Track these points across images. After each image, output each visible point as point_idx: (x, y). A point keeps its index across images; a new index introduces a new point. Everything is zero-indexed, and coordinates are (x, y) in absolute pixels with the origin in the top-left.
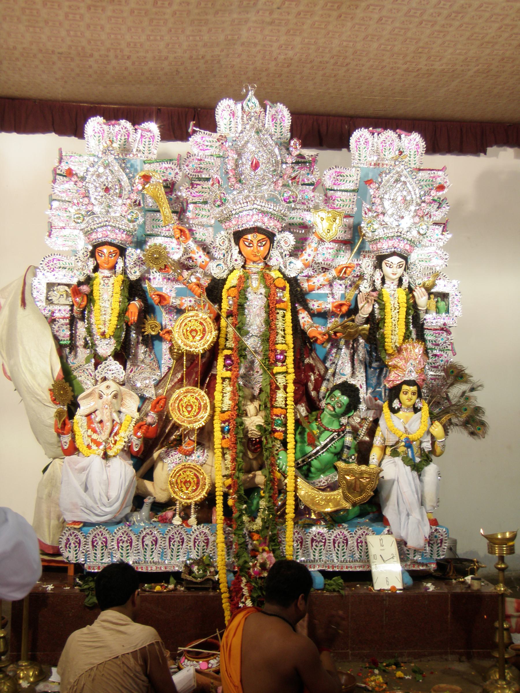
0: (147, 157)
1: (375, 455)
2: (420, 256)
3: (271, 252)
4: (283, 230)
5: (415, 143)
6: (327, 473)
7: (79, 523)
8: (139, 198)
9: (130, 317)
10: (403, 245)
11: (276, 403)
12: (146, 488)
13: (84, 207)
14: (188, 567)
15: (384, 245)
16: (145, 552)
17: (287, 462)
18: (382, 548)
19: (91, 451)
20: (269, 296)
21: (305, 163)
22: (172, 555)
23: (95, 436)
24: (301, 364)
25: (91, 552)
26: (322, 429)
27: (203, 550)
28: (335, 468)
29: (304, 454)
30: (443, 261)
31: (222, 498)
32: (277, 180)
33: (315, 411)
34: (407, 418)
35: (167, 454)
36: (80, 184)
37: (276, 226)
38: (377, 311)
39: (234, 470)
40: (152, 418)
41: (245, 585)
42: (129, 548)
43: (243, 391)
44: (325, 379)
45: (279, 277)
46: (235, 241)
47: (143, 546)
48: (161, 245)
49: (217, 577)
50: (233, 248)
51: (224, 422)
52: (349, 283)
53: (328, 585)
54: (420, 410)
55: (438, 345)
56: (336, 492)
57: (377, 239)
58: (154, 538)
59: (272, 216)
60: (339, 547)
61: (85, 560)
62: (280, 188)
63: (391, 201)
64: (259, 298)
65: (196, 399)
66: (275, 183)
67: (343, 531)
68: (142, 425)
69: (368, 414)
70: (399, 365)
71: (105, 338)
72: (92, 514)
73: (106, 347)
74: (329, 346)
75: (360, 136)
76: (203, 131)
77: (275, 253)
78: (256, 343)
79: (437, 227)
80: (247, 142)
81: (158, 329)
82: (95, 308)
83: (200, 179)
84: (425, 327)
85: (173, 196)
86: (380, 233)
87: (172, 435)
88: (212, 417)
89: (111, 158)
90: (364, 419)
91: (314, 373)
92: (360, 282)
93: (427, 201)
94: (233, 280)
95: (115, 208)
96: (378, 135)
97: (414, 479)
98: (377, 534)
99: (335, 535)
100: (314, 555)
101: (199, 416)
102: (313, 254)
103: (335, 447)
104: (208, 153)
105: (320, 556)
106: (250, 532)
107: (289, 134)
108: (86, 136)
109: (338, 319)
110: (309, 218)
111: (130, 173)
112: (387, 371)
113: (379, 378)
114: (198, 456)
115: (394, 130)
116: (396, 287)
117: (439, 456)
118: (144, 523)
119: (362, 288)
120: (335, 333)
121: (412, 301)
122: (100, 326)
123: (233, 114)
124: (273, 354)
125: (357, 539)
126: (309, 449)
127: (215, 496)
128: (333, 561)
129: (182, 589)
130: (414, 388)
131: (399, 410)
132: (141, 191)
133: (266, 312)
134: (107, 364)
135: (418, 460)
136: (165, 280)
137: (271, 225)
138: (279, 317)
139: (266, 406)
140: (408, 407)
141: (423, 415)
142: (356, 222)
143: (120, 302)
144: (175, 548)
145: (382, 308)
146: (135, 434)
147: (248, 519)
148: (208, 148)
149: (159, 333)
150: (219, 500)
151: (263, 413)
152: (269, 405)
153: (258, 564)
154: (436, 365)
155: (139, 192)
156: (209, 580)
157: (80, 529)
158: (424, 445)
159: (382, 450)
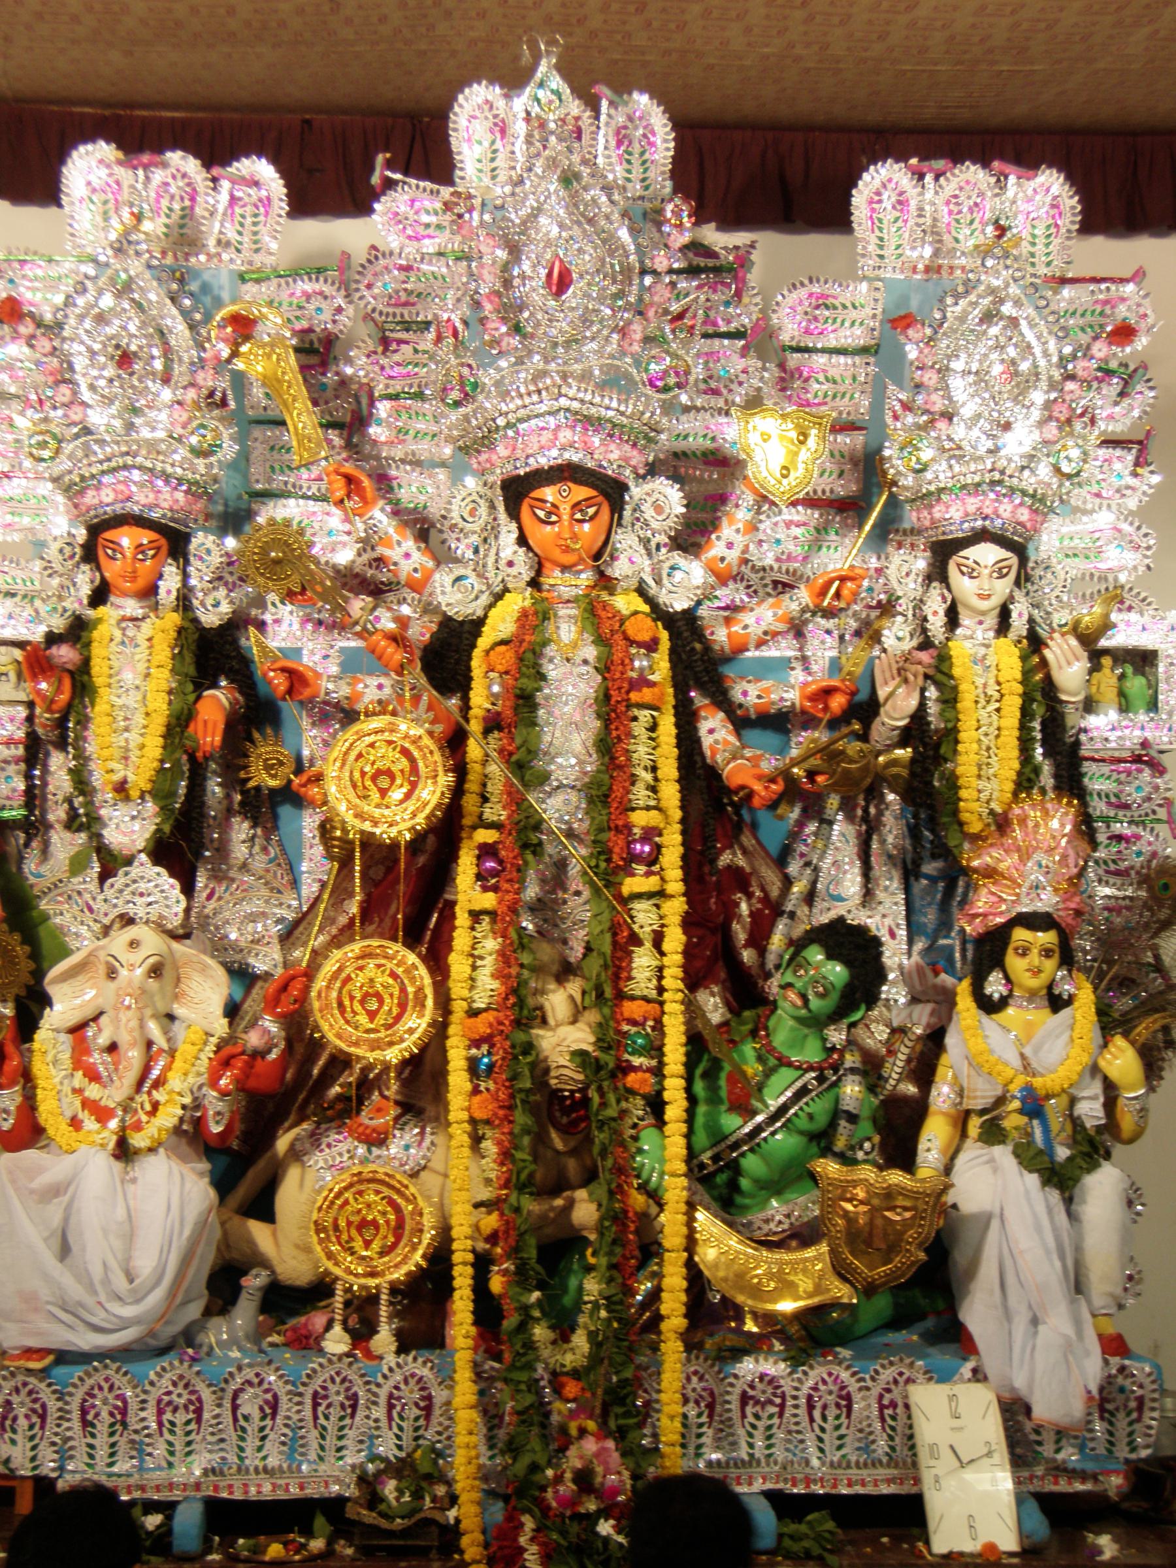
0: (250, 263)
1: (934, 1137)
2: (1066, 542)
3: (614, 537)
4: (652, 470)
5: (1048, 199)
6: (789, 1196)
7: (41, 1352)
8: (223, 384)
9: (200, 734)
10: (1009, 508)
11: (632, 985)
12: (251, 1243)
13: (60, 412)
14: (369, 1483)
15: (952, 510)
16: (242, 1439)
17: (662, 1161)
18: (956, 1423)
19: (81, 1135)
20: (608, 669)
21: (717, 270)
22: (322, 1448)
23: (93, 1091)
24: (706, 869)
25: (79, 1442)
26: (772, 1062)
27: (417, 1429)
28: (813, 1177)
29: (718, 1136)
30: (1138, 556)
31: (469, 1270)
32: (629, 323)
33: (753, 1006)
34: (1029, 1026)
35: (315, 1139)
36: (44, 344)
37: (626, 460)
38: (933, 709)
39: (506, 1185)
40: (266, 1031)
41: (532, 1539)
42: (193, 1426)
43: (532, 951)
44: (781, 913)
45: (636, 613)
46: (507, 509)
47: (235, 1420)
48: (287, 523)
49: (452, 1514)
50: (503, 530)
51: (476, 1043)
52: (854, 624)
53: (791, 1537)
54: (1070, 1001)
55: (1126, 807)
56: (810, 1253)
57: (930, 493)
58: (269, 1396)
59: (614, 431)
60: (824, 1418)
61: (61, 1469)
62: (636, 348)
63: (971, 379)
64: (581, 675)
65: (393, 975)
66: (623, 332)
67: (836, 1370)
68: (233, 1056)
69: (915, 1016)
70: (1002, 866)
71: (127, 799)
72: (81, 1327)
73: (130, 827)
74: (795, 814)
75: (881, 185)
76: (413, 182)
77: (626, 540)
78: (571, 808)
79: (1118, 452)
80: (537, 211)
81: (287, 770)
82: (99, 711)
83: (407, 326)
84: (1084, 753)
85: (330, 377)
86: (941, 473)
87: (332, 1085)
88: (440, 1030)
89: (135, 266)
90: (898, 1031)
91: (749, 896)
92: (886, 622)
93: (1080, 373)
94: (501, 623)
95: (152, 414)
96: (937, 178)
97: (1050, 1211)
98: (939, 1381)
99: (811, 1383)
100: (751, 1446)
101: (401, 1028)
102: (739, 540)
103: (811, 1117)
104: (429, 246)
105: (769, 1447)
106: (554, 1374)
107: (669, 184)
108: (65, 200)
109: (821, 736)
110: (732, 432)
111: (195, 309)
112: (967, 887)
113: (945, 907)
114: (403, 1147)
115: (986, 164)
116: (991, 634)
117: (1130, 1141)
118: (240, 1349)
119: (889, 639)
120: (811, 775)
121: (1039, 677)
122: (114, 765)
123: (502, 129)
124: (621, 842)
125: (881, 1397)
126: (731, 1122)
127: (451, 1266)
128: (807, 1462)
129: (349, 1551)
130: (1047, 938)
131: (1004, 1002)
132: (229, 361)
133: (599, 716)
134: (133, 875)
135: (1062, 1153)
136: (310, 626)
137: (613, 456)
138: (639, 729)
139: (600, 995)
140: (1032, 995)
141: (1078, 1016)
142: (874, 445)
143: (170, 692)
144: (331, 1426)
145: (950, 699)
146: (213, 1083)
147: (551, 1335)
148: (431, 231)
149: (290, 781)
150: (463, 1278)
151: (593, 1016)
152: (608, 992)
153: (568, 1475)
154: (1124, 865)
155: (221, 365)
156: (429, 1522)
157: (44, 1373)
158: (1082, 1108)
159: (955, 1125)
